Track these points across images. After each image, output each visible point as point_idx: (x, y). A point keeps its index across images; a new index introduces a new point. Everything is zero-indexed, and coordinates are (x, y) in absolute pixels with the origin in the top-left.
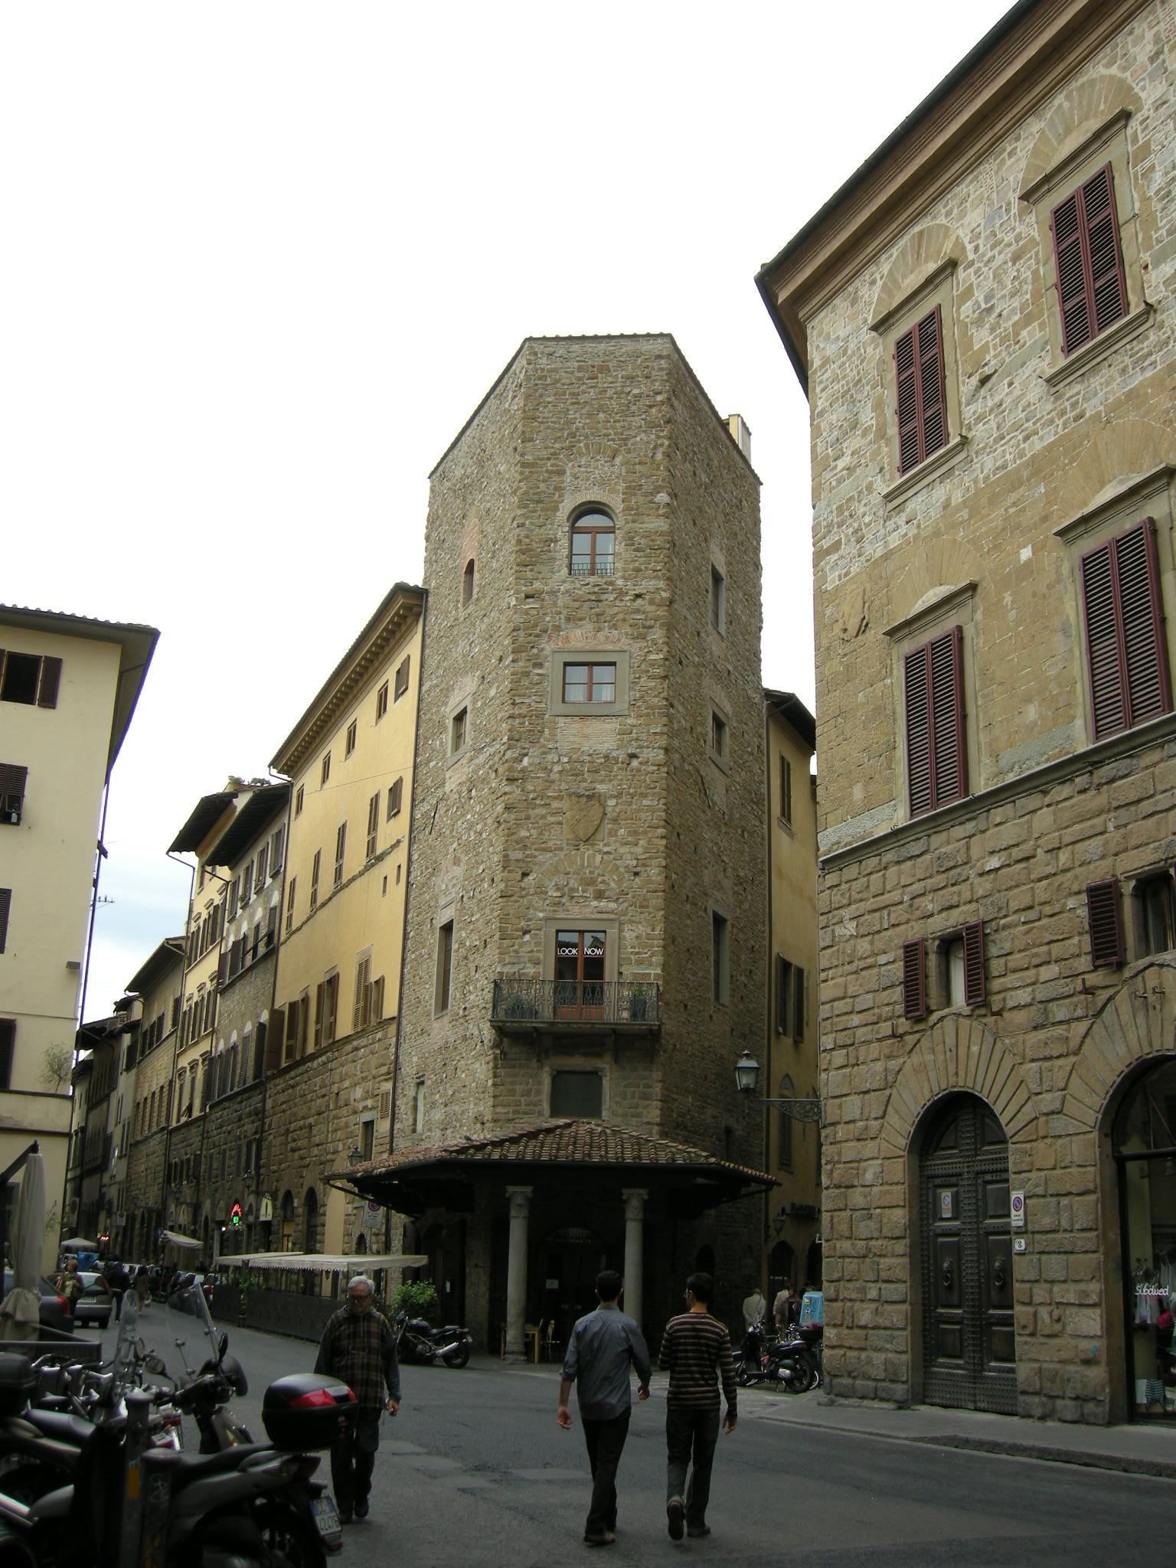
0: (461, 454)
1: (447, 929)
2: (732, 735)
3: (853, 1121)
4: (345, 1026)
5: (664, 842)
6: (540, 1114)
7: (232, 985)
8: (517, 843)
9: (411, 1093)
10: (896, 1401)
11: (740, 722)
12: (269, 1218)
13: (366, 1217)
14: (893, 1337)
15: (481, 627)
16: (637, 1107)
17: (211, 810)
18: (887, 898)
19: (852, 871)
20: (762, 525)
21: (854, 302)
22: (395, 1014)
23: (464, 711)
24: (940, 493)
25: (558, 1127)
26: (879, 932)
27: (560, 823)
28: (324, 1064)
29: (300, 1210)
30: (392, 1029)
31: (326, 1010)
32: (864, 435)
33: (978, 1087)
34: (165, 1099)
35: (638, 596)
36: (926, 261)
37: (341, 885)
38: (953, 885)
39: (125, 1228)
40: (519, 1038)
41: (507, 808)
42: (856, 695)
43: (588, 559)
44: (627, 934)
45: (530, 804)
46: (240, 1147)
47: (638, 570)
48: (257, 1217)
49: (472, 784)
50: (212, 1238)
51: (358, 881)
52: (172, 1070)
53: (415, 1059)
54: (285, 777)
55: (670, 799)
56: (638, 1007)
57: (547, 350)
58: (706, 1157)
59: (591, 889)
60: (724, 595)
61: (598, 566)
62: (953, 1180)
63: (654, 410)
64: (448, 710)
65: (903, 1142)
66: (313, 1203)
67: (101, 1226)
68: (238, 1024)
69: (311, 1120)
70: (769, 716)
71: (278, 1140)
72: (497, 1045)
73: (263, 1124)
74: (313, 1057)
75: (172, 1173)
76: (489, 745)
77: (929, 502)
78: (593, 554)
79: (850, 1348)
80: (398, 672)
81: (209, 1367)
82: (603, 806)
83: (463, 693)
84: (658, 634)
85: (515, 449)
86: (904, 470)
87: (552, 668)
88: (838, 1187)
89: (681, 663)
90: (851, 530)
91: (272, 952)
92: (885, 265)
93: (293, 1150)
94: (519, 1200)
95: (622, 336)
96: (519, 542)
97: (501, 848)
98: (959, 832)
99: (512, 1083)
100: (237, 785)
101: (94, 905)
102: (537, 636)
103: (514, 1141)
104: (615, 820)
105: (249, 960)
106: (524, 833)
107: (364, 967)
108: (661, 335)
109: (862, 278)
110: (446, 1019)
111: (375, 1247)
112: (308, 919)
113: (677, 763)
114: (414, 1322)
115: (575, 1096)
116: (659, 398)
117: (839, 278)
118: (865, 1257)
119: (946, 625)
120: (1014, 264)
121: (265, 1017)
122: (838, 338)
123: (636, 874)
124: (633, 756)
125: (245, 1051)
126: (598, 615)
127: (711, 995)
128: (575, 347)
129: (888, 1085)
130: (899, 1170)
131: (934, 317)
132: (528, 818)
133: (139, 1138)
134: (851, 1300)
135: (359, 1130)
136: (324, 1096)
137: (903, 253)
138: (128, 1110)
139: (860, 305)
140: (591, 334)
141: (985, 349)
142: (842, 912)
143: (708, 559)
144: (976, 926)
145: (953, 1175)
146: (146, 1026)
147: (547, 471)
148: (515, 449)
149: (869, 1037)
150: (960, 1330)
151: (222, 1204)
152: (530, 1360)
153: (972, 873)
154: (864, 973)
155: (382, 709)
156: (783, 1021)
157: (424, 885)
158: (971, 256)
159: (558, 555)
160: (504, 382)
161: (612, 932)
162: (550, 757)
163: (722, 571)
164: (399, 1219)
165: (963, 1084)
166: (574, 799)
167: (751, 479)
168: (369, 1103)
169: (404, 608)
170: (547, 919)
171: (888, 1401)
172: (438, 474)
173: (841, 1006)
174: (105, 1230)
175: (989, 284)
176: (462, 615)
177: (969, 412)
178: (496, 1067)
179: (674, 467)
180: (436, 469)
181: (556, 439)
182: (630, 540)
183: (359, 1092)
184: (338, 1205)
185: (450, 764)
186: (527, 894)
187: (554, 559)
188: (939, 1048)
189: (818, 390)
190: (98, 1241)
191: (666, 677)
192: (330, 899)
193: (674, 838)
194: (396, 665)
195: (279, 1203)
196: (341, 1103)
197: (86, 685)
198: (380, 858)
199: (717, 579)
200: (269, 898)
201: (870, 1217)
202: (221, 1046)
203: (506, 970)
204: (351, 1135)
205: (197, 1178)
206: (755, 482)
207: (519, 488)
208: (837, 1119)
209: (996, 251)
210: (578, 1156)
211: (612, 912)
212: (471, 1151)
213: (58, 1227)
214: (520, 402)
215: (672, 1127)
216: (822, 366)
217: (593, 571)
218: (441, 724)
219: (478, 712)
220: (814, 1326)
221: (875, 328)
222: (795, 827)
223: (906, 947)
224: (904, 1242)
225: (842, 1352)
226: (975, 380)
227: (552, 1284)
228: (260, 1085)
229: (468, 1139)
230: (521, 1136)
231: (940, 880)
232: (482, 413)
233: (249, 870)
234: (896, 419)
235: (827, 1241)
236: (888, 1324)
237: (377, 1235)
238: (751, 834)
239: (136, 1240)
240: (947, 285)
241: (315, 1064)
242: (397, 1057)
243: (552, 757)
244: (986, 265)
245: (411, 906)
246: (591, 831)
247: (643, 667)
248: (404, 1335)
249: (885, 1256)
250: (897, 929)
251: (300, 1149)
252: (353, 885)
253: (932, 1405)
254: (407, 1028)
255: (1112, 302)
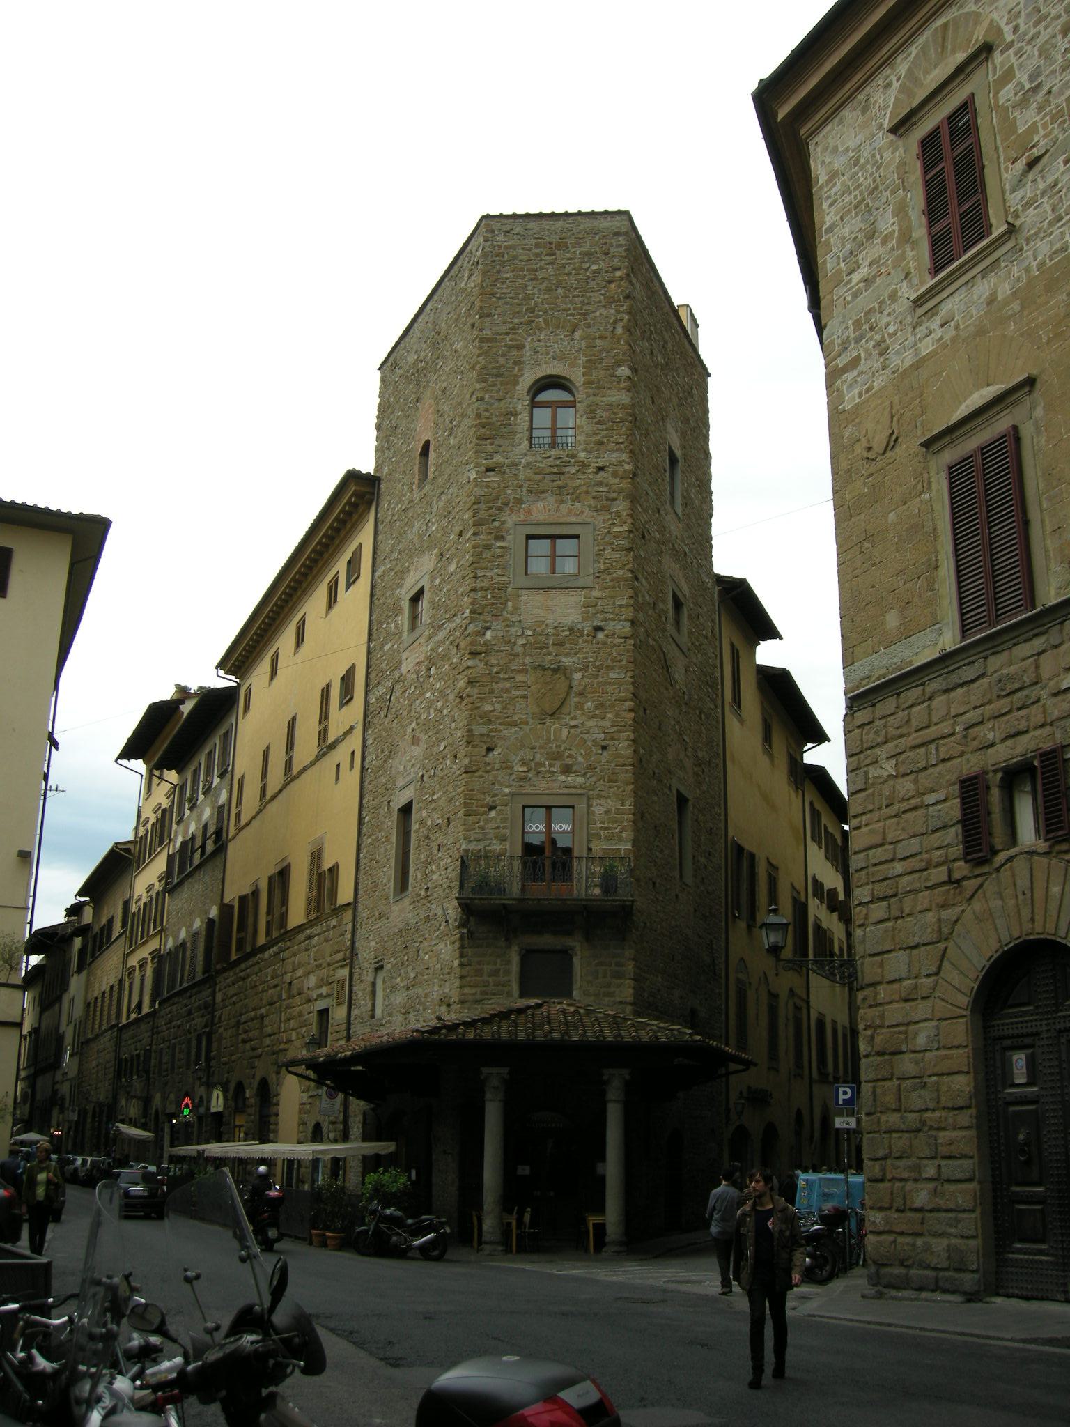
0: (414, 340)
1: (406, 810)
2: (690, 617)
3: (899, 980)
4: (297, 915)
5: (632, 715)
6: (509, 994)
7: (180, 884)
8: (481, 717)
9: (370, 978)
10: (965, 1293)
11: (696, 604)
12: (220, 1109)
13: (324, 1105)
14: (958, 1221)
15: (438, 505)
16: (609, 986)
17: (158, 715)
18: (932, 732)
19: (889, 705)
20: (710, 415)
21: (865, 110)
22: (351, 900)
23: (421, 592)
24: (982, 289)
25: (529, 1007)
26: (925, 769)
27: (525, 697)
28: (276, 954)
29: (252, 1101)
30: (348, 915)
31: (277, 901)
32: (884, 242)
33: (1062, 933)
34: (115, 998)
35: (601, 469)
36: (954, 51)
37: (291, 775)
38: (1019, 709)
39: (77, 1123)
40: (487, 916)
41: (471, 682)
42: (885, 516)
43: (548, 433)
44: (596, 810)
45: (494, 678)
46: (189, 1041)
47: (601, 443)
48: (208, 1109)
49: (431, 661)
50: (163, 1130)
51: (309, 771)
52: (124, 969)
53: (373, 944)
54: (232, 678)
55: (637, 672)
56: (609, 882)
57: (504, 228)
58: (691, 1034)
59: (558, 763)
60: (679, 476)
61: (559, 440)
62: (1027, 1041)
63: (613, 286)
64: (403, 592)
65: (964, 1000)
66: (266, 1094)
67: (54, 1122)
68: (186, 922)
69: (263, 1011)
70: (720, 602)
71: (229, 1033)
72: (463, 924)
73: (213, 1017)
74: (264, 948)
75: (123, 1068)
76: (448, 620)
77: (966, 302)
78: (554, 428)
79: (902, 1234)
80: (349, 562)
81: (246, 1320)
82: (569, 679)
83: (420, 572)
84: (622, 506)
85: (473, 326)
86: (936, 270)
87: (514, 541)
88: (879, 1054)
89: (643, 537)
90: (872, 343)
91: (221, 849)
92: (902, 66)
93: (244, 1041)
94: (495, 1082)
95: (580, 213)
96: (478, 416)
97: (465, 722)
98: (1024, 649)
99: (479, 963)
100: (183, 692)
101: (45, 794)
102: (499, 509)
103: (486, 1021)
104: (581, 694)
105: (197, 859)
106: (488, 707)
107: (317, 856)
108: (619, 212)
109: (874, 84)
110: (406, 901)
111: (332, 1135)
112: (258, 813)
113: (642, 637)
114: (388, 1212)
115: (545, 974)
116: (618, 274)
117: (848, 86)
118: (918, 1131)
119: (1001, 424)
120: (1065, 36)
121: (214, 912)
122: (847, 149)
123: (604, 748)
124: (598, 629)
125: (194, 946)
126: (560, 487)
127: (677, 874)
128: (533, 225)
129: (942, 936)
130: (960, 1031)
131: (967, 107)
132: (492, 692)
133: (97, 1031)
134: (901, 1180)
135: (314, 1018)
136: (276, 986)
137: (924, 50)
138: (79, 1010)
139: (874, 110)
140: (549, 211)
141: (1033, 129)
142: (877, 751)
143: (665, 439)
144: (1053, 751)
145: (1027, 1035)
146: (96, 929)
147: (506, 346)
148: (473, 326)
149: (916, 885)
150: (1042, 1211)
151: (172, 1097)
152: (508, 1250)
153: (1044, 694)
154: (906, 816)
155: (332, 599)
156: (737, 905)
157: (379, 768)
158: (1009, 37)
159: (518, 429)
160: (459, 263)
161: (581, 806)
162: (513, 631)
163: (678, 453)
164: (358, 1106)
165: (1042, 928)
166: (539, 672)
167: (700, 369)
168: (324, 990)
169: (355, 497)
170: (513, 795)
171: (953, 1292)
172: (389, 365)
173: (878, 854)
174: (58, 1125)
175: (1034, 61)
176: (417, 496)
177: (1014, 200)
178: (462, 947)
179: (634, 342)
180: (387, 359)
181: (515, 314)
182: (591, 413)
183: (313, 980)
184: (292, 1093)
185: (406, 645)
186: (493, 769)
187: (515, 432)
188: (1010, 891)
189: (825, 206)
190: (52, 1136)
191: (631, 549)
192: (280, 791)
193: (641, 712)
194: (348, 555)
195: (230, 1095)
196: (294, 991)
197: (38, 575)
198: (332, 746)
199: (673, 460)
200: (217, 797)
201: (924, 1085)
202: (170, 944)
203: (472, 847)
204: (305, 1024)
205: (147, 1072)
206: (703, 373)
207: (478, 362)
208: (878, 979)
209: (1041, 27)
210: (556, 1035)
211: (580, 787)
212: (444, 1031)
213: (9, 1119)
214: (477, 278)
215: (645, 1005)
216: (831, 179)
217: (554, 445)
218: (397, 609)
219: (436, 589)
220: (836, 1209)
221: (894, 130)
222: (744, 714)
223: (962, 782)
224: (969, 1112)
225: (891, 1238)
226: (1021, 165)
227: (524, 1170)
228: (209, 978)
229: (439, 1018)
230: (493, 1016)
231: (1003, 705)
232: (435, 297)
233: (196, 773)
234: (924, 220)
235: (868, 1114)
236: (951, 1205)
237: (333, 1123)
238: (707, 716)
239: (88, 1133)
240: (981, 72)
241: (266, 955)
242: (353, 943)
243: (516, 630)
244: (1029, 43)
245: (365, 791)
246: (557, 705)
247: (607, 539)
248: (377, 1226)
249: (944, 1129)
250: (949, 764)
251: (251, 1040)
252: (304, 776)
253: (1008, 1296)
254: (363, 913)
255: (975, 224)
